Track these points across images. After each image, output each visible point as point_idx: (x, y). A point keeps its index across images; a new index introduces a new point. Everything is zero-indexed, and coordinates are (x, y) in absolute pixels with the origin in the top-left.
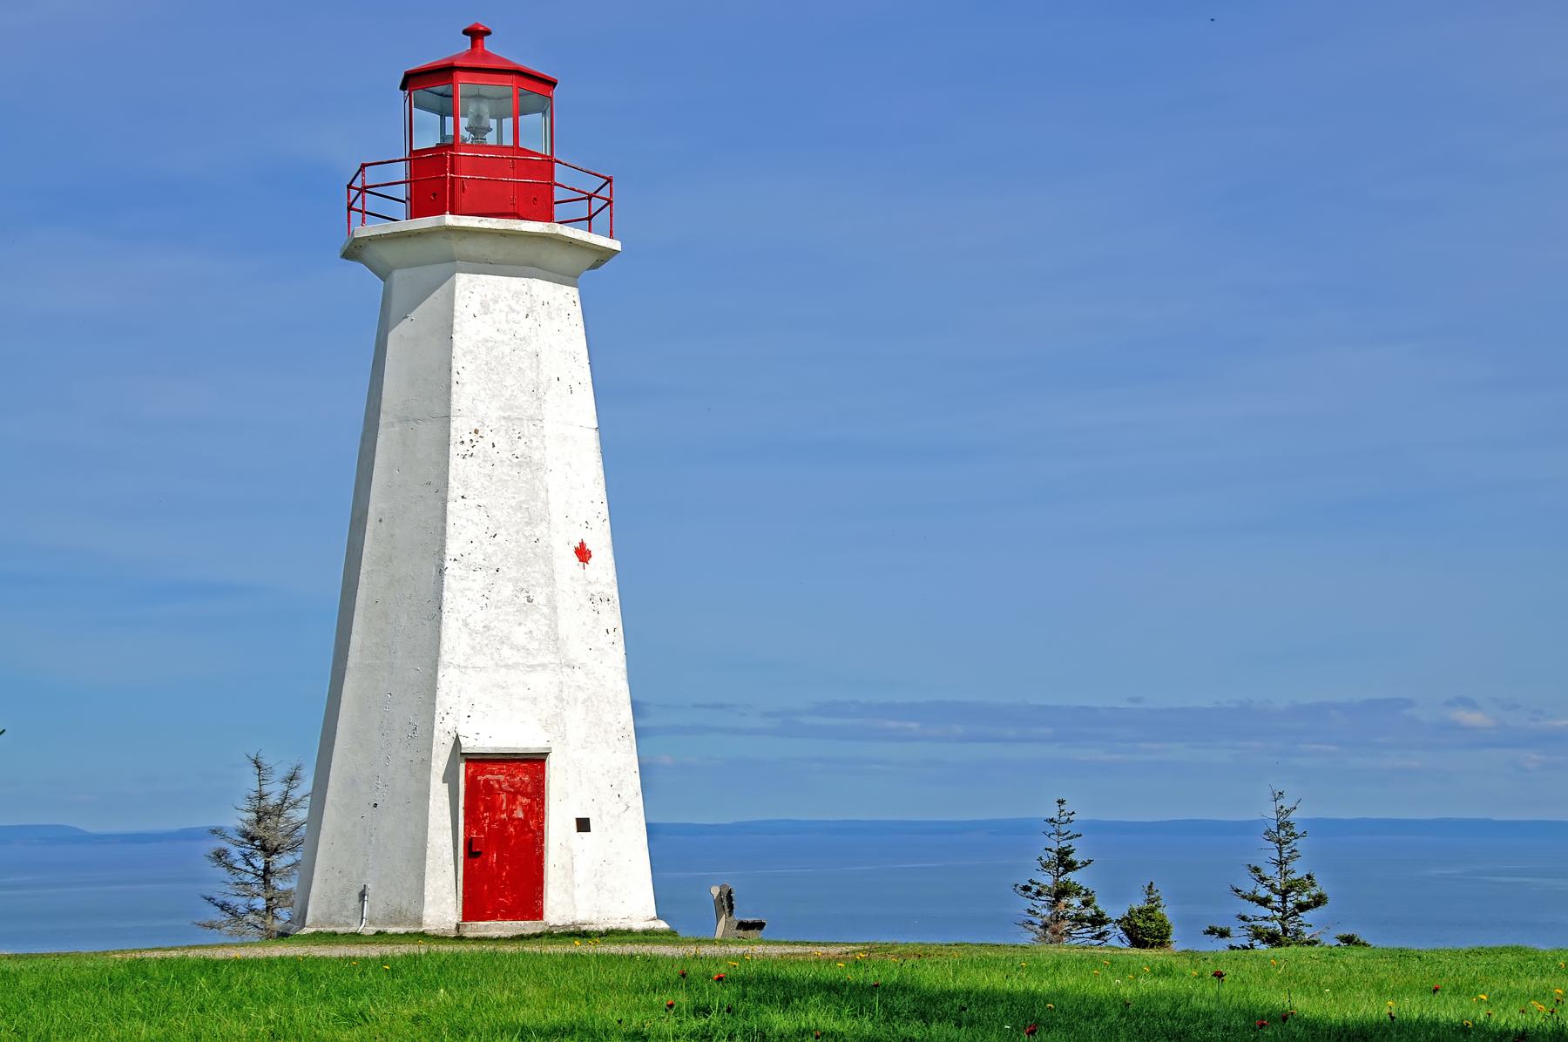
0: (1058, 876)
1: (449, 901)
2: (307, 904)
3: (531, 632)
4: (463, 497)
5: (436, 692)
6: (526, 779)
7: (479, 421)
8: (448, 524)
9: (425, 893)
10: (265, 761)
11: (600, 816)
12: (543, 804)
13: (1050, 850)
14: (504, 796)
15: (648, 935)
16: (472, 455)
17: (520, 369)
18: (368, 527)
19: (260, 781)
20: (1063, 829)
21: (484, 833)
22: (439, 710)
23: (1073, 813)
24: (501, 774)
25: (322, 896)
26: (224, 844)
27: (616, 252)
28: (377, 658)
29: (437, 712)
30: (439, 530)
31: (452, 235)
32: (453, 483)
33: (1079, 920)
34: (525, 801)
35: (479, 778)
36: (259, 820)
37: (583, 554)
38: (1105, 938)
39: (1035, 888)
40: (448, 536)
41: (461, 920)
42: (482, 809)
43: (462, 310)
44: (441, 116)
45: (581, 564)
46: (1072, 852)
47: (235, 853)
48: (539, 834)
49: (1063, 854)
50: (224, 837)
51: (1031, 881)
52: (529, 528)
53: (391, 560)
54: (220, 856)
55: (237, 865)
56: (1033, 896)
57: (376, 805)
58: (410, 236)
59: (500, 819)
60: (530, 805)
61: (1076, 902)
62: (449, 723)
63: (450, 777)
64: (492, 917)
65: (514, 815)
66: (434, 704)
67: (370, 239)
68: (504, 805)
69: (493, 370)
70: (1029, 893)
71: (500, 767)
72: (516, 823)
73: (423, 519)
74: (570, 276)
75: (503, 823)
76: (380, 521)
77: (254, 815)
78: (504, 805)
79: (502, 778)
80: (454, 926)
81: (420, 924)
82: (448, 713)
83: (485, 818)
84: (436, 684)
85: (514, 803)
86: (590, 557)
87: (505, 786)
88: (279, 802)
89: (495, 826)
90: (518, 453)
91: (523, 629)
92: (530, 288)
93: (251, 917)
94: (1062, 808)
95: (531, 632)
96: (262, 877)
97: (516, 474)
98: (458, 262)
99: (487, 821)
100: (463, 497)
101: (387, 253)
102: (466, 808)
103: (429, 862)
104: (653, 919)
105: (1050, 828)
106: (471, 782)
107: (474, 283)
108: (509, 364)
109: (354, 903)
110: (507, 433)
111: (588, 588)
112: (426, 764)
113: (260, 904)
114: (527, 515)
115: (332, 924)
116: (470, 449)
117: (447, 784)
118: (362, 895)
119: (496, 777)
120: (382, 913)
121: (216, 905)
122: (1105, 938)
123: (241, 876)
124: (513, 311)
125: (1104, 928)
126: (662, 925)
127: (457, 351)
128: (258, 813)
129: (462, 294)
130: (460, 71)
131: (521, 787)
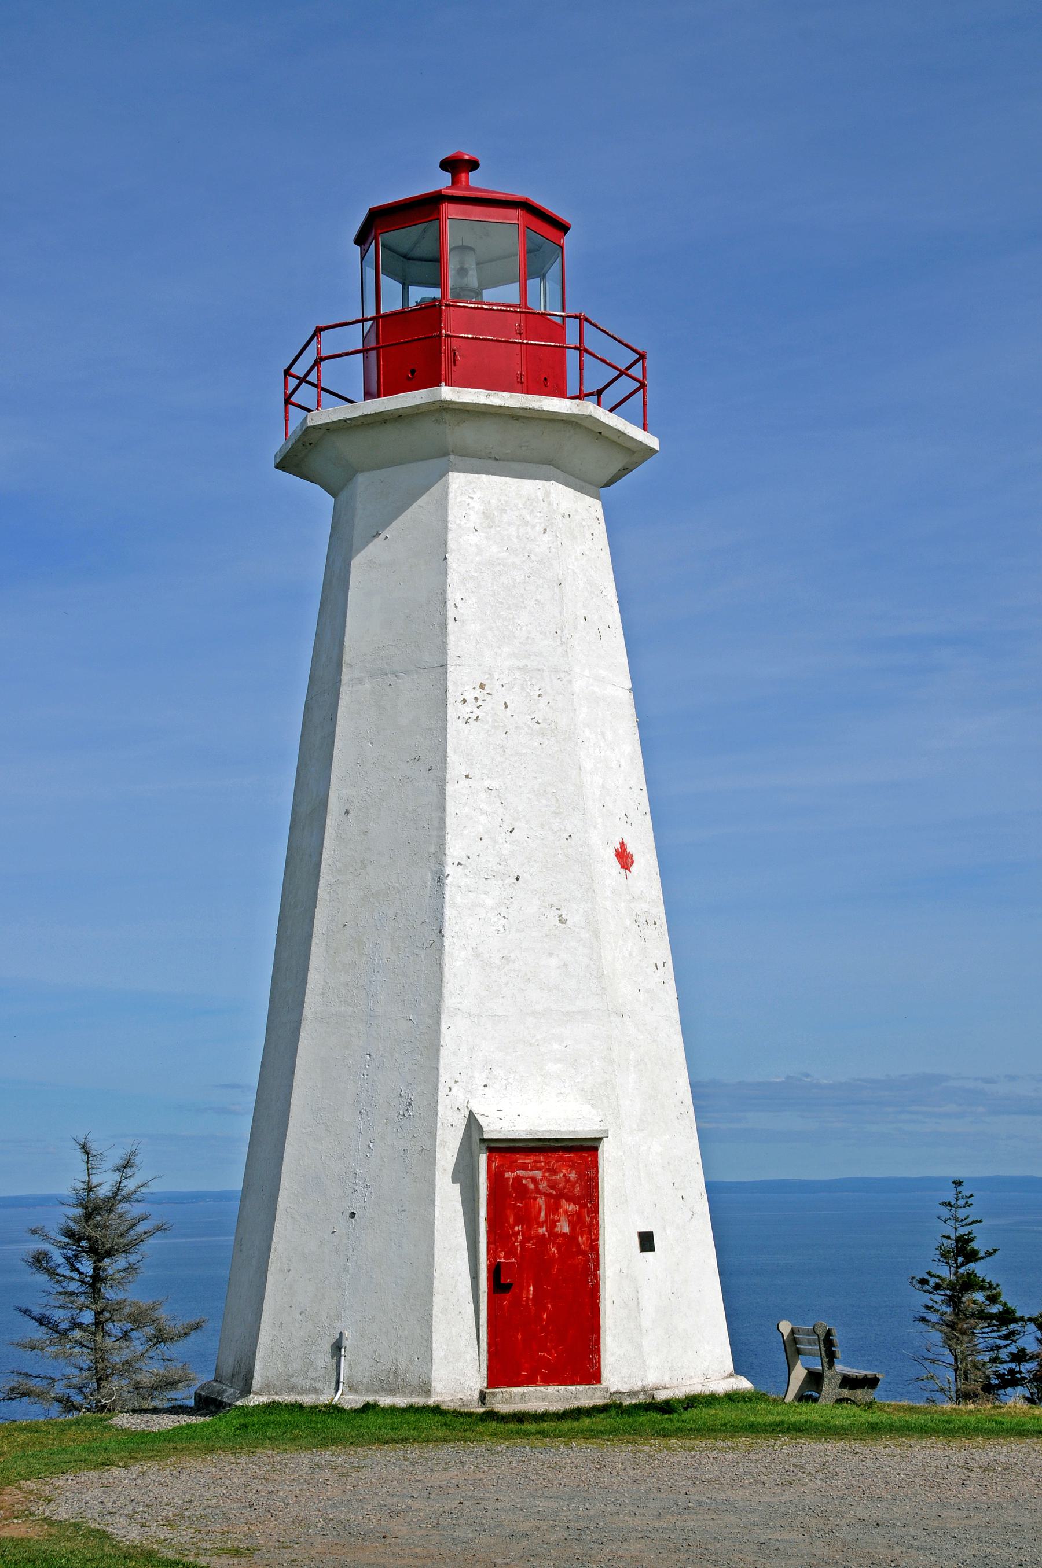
0: (958, 1267)
1: (468, 1357)
2: (254, 1359)
3: (565, 965)
4: (467, 776)
5: (438, 1050)
6: (573, 1175)
7: (485, 673)
8: (448, 812)
9: (434, 1346)
10: (94, 1147)
11: (664, 1229)
12: (597, 1212)
13: (948, 1238)
14: (541, 1201)
15: (733, 1397)
16: (477, 719)
17: (538, 601)
18: (328, 822)
19: (88, 1169)
20: (961, 1213)
21: (515, 1256)
22: (444, 1077)
23: (972, 1196)
24: (539, 1169)
25: (276, 1348)
26: (45, 1246)
27: (652, 451)
28: (349, 1004)
29: (442, 1079)
30: (436, 823)
31: (447, 417)
32: (452, 757)
33: (983, 1316)
34: (571, 1207)
35: (507, 1175)
36: (88, 1216)
37: (624, 858)
38: (1015, 1338)
39: (933, 1281)
40: (448, 830)
41: (485, 1385)
42: (511, 1220)
43: (458, 522)
44: (404, 285)
45: (623, 871)
46: (972, 1240)
47: (57, 1257)
48: (592, 1256)
49: (963, 1242)
50: (46, 1237)
51: (929, 1273)
52: (558, 820)
53: (364, 866)
54: (40, 1260)
55: (60, 1271)
56: (931, 1290)
57: (353, 1215)
58: (385, 421)
59: (538, 1236)
60: (579, 1214)
61: (979, 1296)
62: (459, 1094)
63: (464, 1174)
64: (530, 1381)
65: (558, 1229)
66: (437, 1069)
67: (330, 428)
68: (543, 1214)
69: (502, 603)
70: (926, 1287)
71: (536, 1158)
72: (560, 1240)
73: (410, 808)
74: (591, 483)
75: (541, 1240)
76: (347, 812)
77: (80, 1211)
78: (543, 1214)
79: (538, 1174)
80: (476, 1395)
81: (428, 1393)
82: (456, 1082)
83: (517, 1234)
84: (439, 1039)
85: (556, 1212)
86: (632, 862)
87: (543, 1186)
88: (110, 1194)
89: (530, 1245)
90: (539, 717)
91: (554, 961)
92: (547, 494)
93: (77, 1334)
94: (959, 1189)
95: (565, 965)
96: (90, 1285)
97: (536, 744)
98: (452, 457)
99: (519, 1238)
100: (467, 776)
101: (349, 447)
102: (489, 1220)
103: (437, 1299)
104: (731, 1375)
105: (945, 1212)
106: (496, 1180)
107: (473, 485)
108: (522, 595)
109: (324, 1359)
110: (523, 689)
111: (632, 905)
112: (428, 1156)
113: (87, 1317)
114: (554, 800)
115: (291, 1389)
116: (475, 710)
117: (459, 1184)
118: (337, 1347)
119: (531, 1173)
120: (367, 1374)
121: (33, 1318)
122: (1015, 1338)
123: (65, 1284)
124: (527, 523)
125: (1012, 1327)
126: (744, 1384)
127: (453, 577)
128: (86, 1208)
129: (458, 500)
130: (449, 202)
131: (565, 1188)
